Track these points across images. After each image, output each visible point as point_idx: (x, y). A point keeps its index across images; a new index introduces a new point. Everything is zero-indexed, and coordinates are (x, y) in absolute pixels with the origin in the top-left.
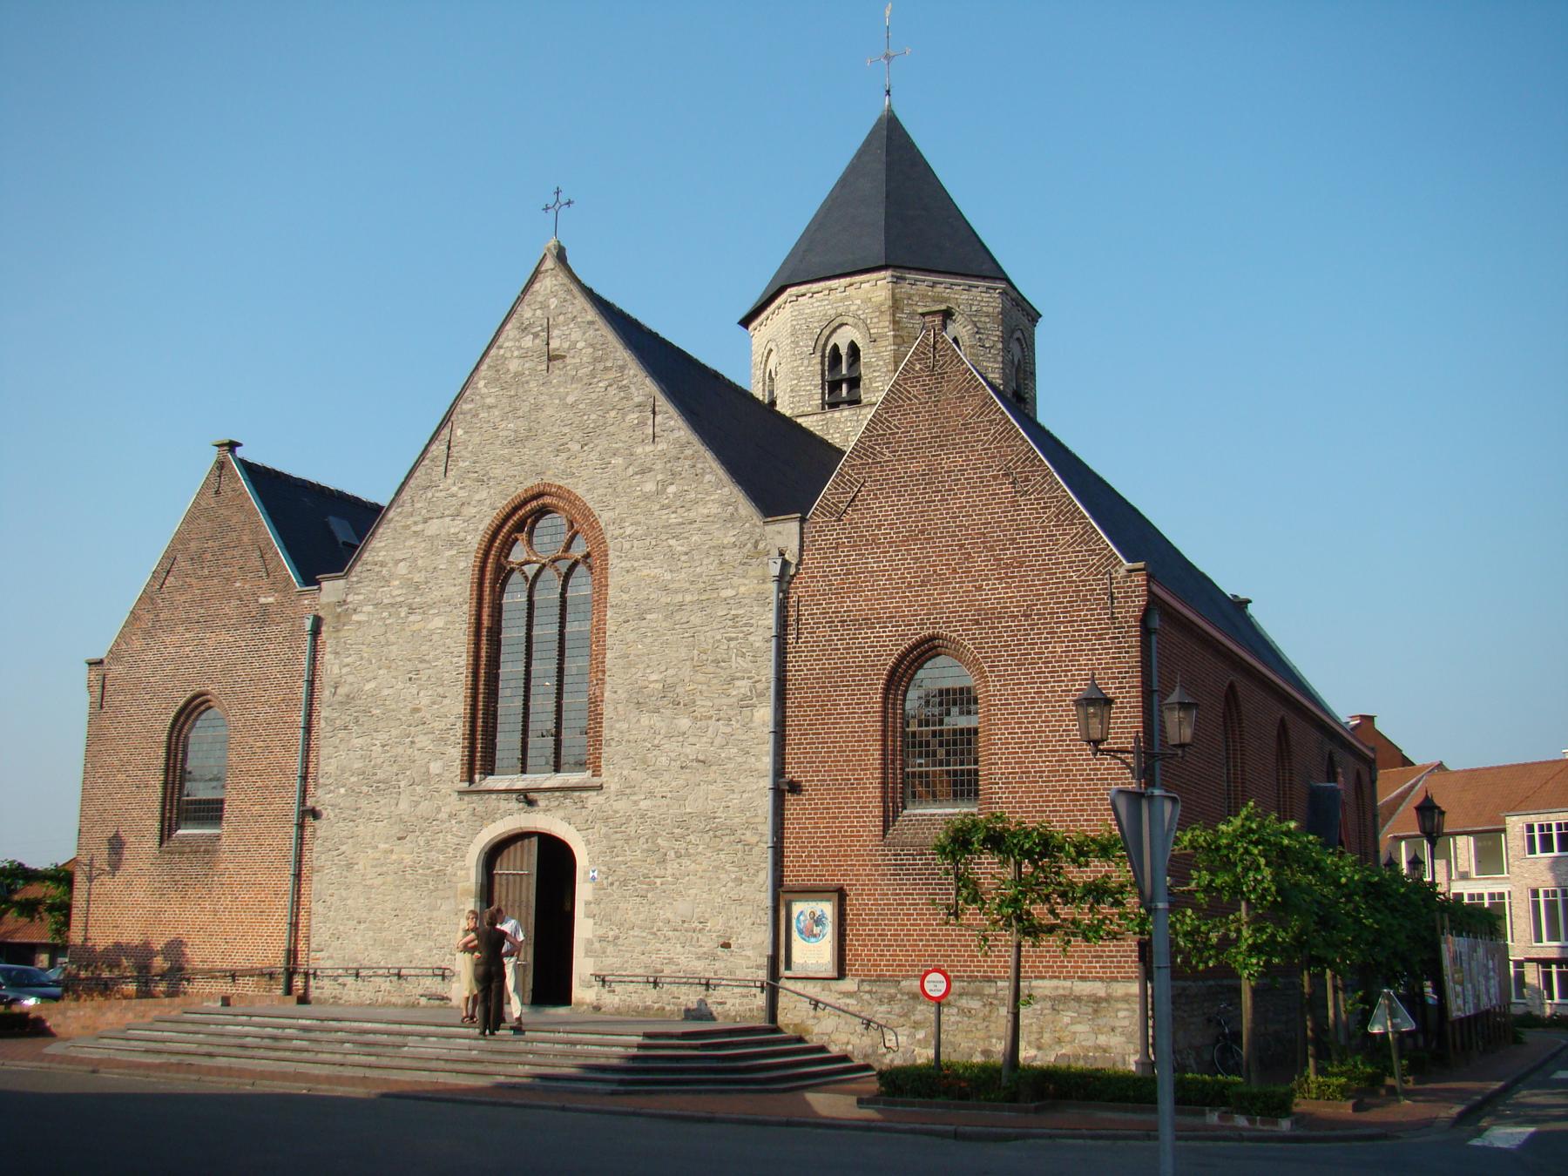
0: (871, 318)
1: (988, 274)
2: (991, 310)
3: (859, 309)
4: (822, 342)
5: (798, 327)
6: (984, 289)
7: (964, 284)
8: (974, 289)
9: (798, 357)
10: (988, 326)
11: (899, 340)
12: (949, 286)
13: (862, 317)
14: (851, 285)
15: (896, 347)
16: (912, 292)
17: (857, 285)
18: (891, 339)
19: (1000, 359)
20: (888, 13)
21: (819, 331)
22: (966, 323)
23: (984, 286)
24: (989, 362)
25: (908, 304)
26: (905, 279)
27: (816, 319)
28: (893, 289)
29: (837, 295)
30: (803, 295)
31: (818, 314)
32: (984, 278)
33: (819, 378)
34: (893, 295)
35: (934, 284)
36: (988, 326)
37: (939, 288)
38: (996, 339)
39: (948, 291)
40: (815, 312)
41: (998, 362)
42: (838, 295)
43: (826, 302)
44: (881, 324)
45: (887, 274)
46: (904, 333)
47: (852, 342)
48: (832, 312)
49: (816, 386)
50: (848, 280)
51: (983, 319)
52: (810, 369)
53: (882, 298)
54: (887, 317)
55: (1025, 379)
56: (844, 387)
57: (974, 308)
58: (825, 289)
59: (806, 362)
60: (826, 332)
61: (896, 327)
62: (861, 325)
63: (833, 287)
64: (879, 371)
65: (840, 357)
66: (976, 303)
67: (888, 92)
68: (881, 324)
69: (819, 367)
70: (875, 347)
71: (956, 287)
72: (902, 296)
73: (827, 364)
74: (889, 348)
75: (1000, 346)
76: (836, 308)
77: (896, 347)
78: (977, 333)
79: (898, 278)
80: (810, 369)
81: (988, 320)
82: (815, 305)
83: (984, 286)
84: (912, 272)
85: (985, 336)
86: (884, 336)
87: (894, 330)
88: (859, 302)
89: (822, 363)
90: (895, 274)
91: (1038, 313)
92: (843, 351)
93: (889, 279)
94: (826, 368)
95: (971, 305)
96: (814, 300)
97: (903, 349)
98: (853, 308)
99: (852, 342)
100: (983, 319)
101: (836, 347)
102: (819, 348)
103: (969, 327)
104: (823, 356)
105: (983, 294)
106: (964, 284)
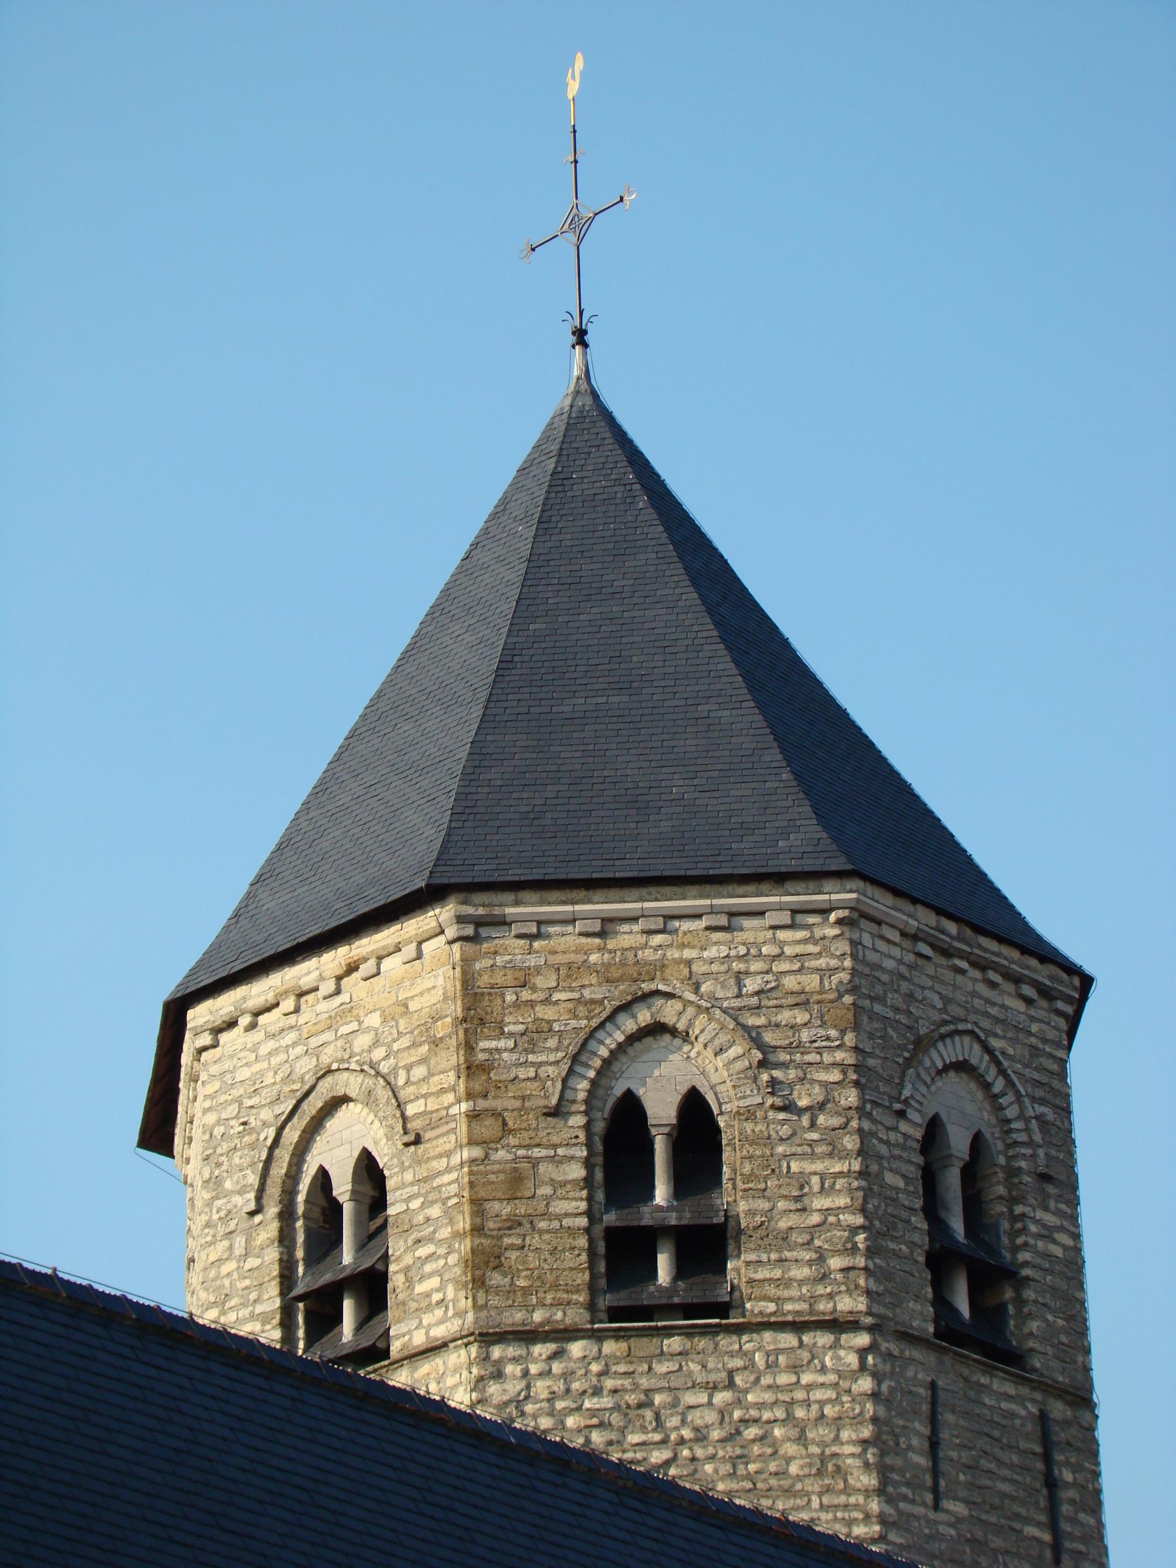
0: (409, 1068)
1: (794, 865)
2: (811, 982)
3: (376, 1043)
4: (280, 1169)
5: (218, 1131)
6: (785, 918)
7: (712, 911)
8: (747, 923)
9: (221, 1230)
10: (805, 1036)
11: (488, 1128)
12: (659, 923)
13: (384, 1068)
14: (352, 968)
15: (477, 1152)
16: (532, 961)
17: (367, 968)
18: (463, 1127)
19: (850, 1142)
20: (573, 88)
21: (271, 1133)
22: (723, 1038)
23: (781, 908)
24: (812, 1156)
25: (517, 1005)
26: (502, 922)
27: (267, 1095)
28: (466, 961)
29: (317, 1009)
30: (231, 1024)
31: (269, 1079)
32: (780, 879)
33: (273, 1289)
34: (468, 982)
35: (606, 927)
36: (805, 1036)
37: (627, 937)
38: (835, 1076)
39: (658, 939)
40: (261, 1073)
41: (844, 1155)
42: (324, 1006)
43: (291, 1037)
44: (436, 1082)
45: (444, 913)
46: (505, 1102)
47: (321, 1166)
48: (306, 1067)
49: (265, 1318)
50: (333, 959)
51: (784, 1016)
52: (252, 1262)
53: (437, 995)
54: (451, 1057)
55: (1013, 1201)
56: (348, 1307)
57: (751, 985)
58: (285, 993)
59: (240, 1241)
60: (292, 1135)
61: (477, 1086)
62: (383, 1094)
63: (306, 982)
64: (430, 1239)
65: (337, 1208)
66: (756, 966)
67: (580, 336)
68: (436, 1082)
69: (273, 1254)
70: (419, 1162)
71: (686, 925)
72: (499, 979)
73: (300, 1238)
74: (456, 1159)
75: (850, 1097)
76: (317, 1052)
77: (477, 1152)
78: (763, 1064)
79: (479, 923)
80: (252, 1262)
81: (801, 1017)
82: (264, 1050)
83: (781, 908)
84: (526, 895)
85: (792, 1074)
86: (438, 1120)
87: (470, 1096)
88: (374, 1020)
89: (285, 1238)
90: (469, 910)
91: (1072, 969)
92: (342, 1188)
93: (451, 932)
94: (300, 1253)
95: (739, 977)
96: (257, 1036)
97: (501, 1154)
98: (362, 1042)
99: (321, 1166)
100: (784, 1016)
101: (323, 1178)
102: (274, 1191)
103: (733, 1052)
104: (287, 1215)
105: (782, 935)
106: (712, 911)
